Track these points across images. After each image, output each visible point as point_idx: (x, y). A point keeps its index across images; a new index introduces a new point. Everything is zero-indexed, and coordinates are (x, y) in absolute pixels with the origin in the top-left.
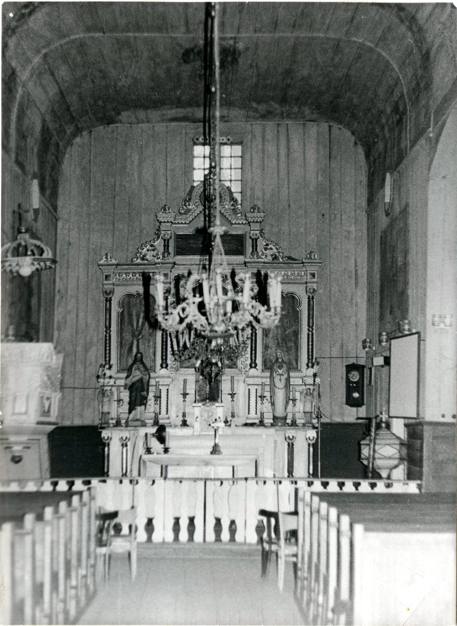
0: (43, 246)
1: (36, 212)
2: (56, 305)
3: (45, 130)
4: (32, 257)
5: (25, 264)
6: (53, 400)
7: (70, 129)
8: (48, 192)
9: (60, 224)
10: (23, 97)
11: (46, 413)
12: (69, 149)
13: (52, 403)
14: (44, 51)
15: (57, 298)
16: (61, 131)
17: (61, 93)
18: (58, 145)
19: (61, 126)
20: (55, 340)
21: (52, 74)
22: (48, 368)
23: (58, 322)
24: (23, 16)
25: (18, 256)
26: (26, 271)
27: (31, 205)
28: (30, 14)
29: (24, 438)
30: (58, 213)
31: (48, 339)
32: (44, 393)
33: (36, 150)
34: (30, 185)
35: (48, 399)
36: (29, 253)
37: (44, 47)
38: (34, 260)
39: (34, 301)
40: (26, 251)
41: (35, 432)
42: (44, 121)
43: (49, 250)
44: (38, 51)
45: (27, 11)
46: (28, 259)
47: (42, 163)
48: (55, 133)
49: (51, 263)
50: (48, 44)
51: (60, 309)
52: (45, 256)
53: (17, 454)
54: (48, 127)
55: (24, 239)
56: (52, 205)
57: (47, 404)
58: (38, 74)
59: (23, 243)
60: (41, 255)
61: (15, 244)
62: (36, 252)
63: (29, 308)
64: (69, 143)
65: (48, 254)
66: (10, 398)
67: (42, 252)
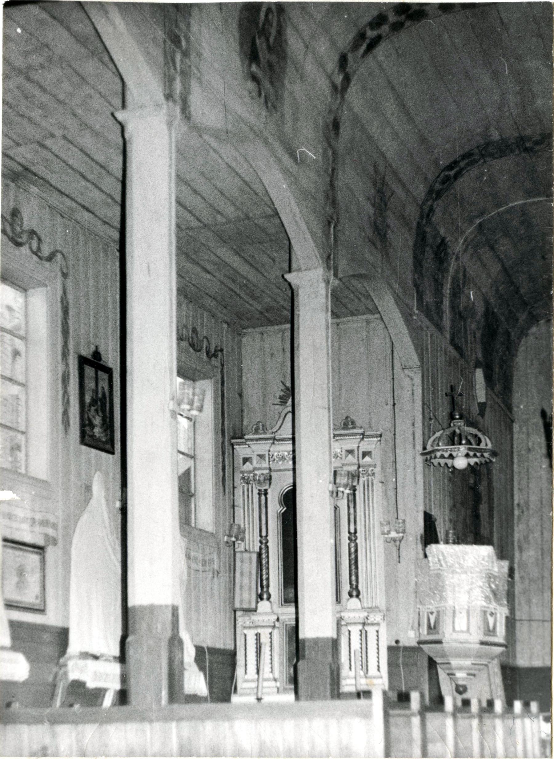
0: (480, 435)
1: (482, 406)
2: (515, 521)
3: (488, 313)
4: (467, 446)
5: (460, 454)
6: (498, 615)
7: (523, 317)
8: (498, 387)
9: (516, 427)
10: (457, 271)
11: (491, 632)
12: (523, 341)
13: (498, 619)
14: (478, 221)
15: (516, 512)
16: (512, 318)
17: (505, 270)
18: (508, 334)
19: (510, 312)
20: (495, 540)
21: (492, 248)
22: (490, 577)
23: (519, 541)
24: (447, 178)
25: (453, 444)
26: (461, 463)
27: (474, 397)
28: (456, 177)
29: (468, 663)
30: (513, 413)
31: (488, 542)
32: (488, 607)
33: (478, 335)
34: (473, 373)
35: (492, 614)
36: (464, 442)
37: (478, 217)
38: (470, 449)
39: (483, 509)
40: (461, 440)
41: (479, 656)
42: (487, 303)
43: (488, 440)
44: (471, 221)
45: (452, 173)
46: (463, 449)
47: (488, 350)
48: (503, 319)
49: (490, 455)
50: (482, 213)
51: (520, 526)
52: (482, 446)
53: (460, 683)
54: (493, 313)
55: (459, 425)
56: (506, 405)
57: (491, 620)
58: (473, 246)
59: (458, 431)
60: (479, 445)
61: (448, 432)
62: (472, 441)
63: (476, 516)
64: (523, 333)
65: (486, 445)
66: (449, 613)
67: (479, 442)
